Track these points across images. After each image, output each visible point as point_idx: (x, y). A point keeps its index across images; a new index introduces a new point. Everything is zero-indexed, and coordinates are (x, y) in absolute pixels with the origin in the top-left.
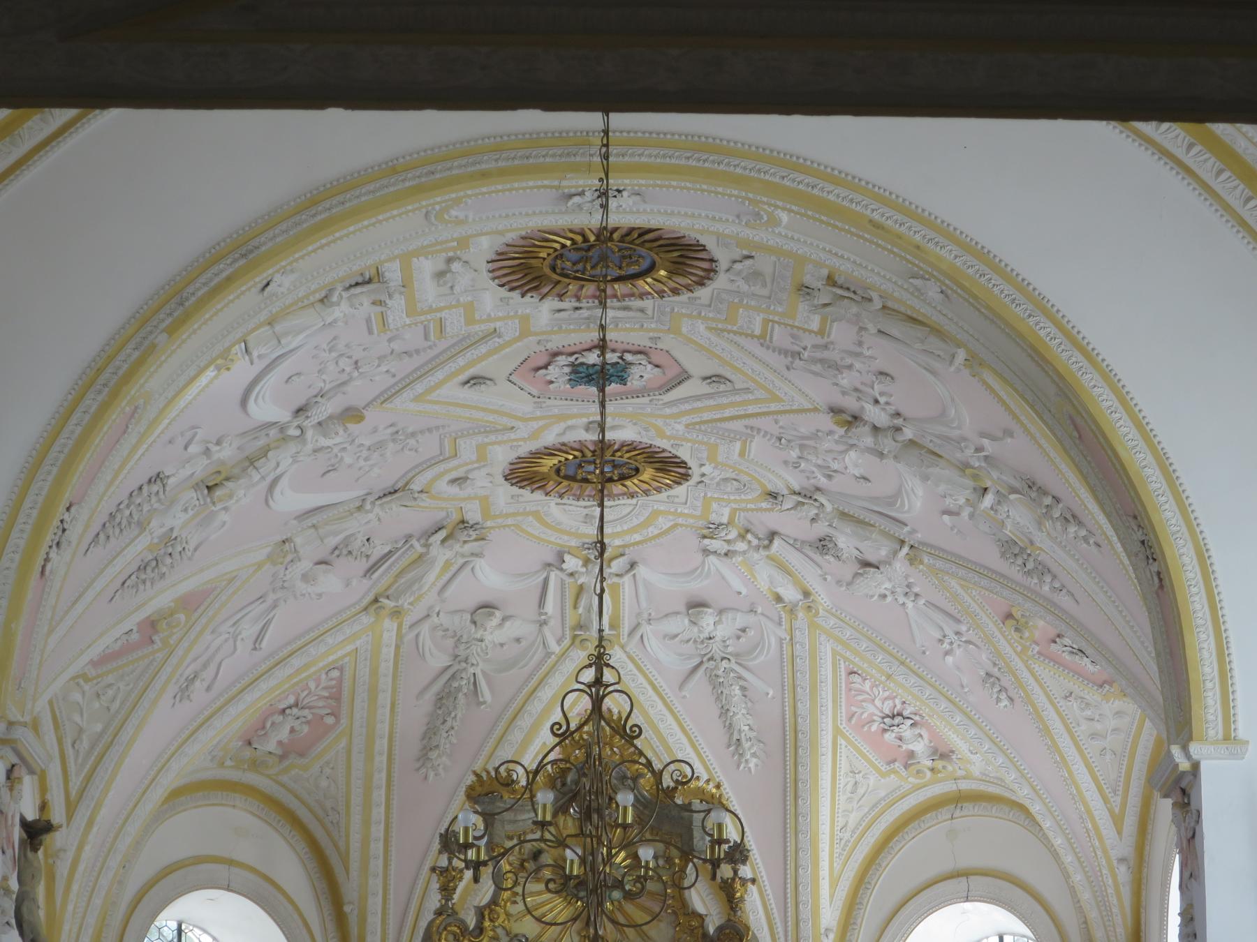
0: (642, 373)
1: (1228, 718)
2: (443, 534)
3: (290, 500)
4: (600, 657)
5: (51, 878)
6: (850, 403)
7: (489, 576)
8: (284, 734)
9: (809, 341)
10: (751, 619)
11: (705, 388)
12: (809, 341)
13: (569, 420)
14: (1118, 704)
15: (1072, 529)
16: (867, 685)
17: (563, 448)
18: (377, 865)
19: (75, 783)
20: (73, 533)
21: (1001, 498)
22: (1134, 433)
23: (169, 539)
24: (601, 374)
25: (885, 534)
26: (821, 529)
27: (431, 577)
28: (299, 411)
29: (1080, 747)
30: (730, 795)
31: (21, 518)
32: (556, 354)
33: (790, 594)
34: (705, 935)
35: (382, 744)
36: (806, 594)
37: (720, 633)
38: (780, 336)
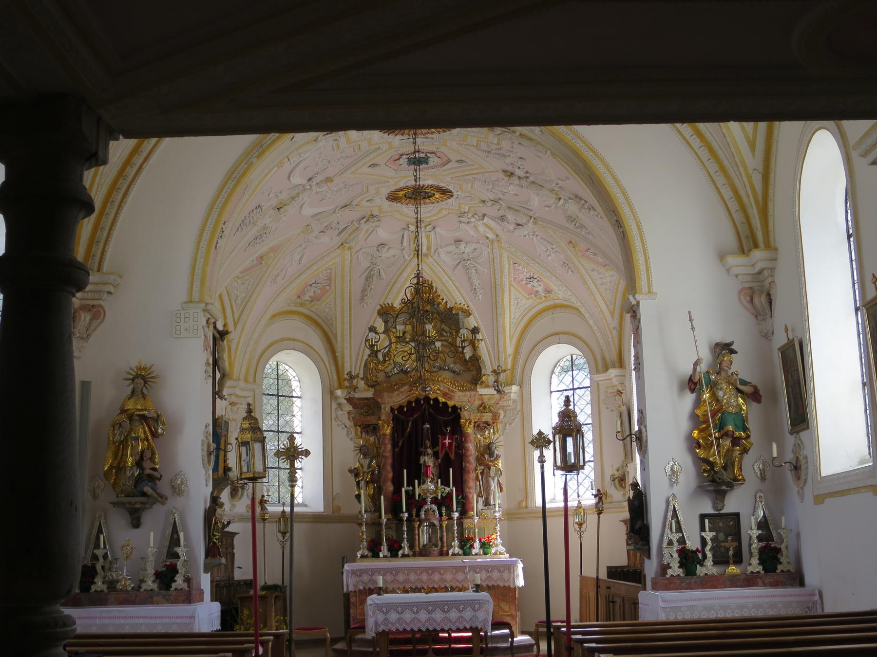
0: (433, 161)
1: (649, 285)
2: (365, 220)
3: (308, 211)
4: (418, 274)
5: (229, 349)
6: (510, 169)
7: (382, 234)
8: (311, 294)
9: (494, 147)
10: (478, 245)
11: (457, 165)
12: (494, 147)
13: (405, 178)
14: (611, 273)
15: (592, 212)
16: (520, 268)
17: (407, 188)
18: (347, 338)
19: (236, 315)
20: (227, 232)
21: (566, 201)
22: (612, 181)
23: (265, 228)
24: (417, 161)
25: (526, 215)
26: (501, 213)
27: (361, 235)
28: (310, 179)
29: (598, 289)
30: (473, 309)
31: (207, 228)
32: (402, 155)
33: (491, 236)
34: (465, 360)
35: (347, 295)
36: (497, 236)
37: (467, 251)
38: (483, 146)
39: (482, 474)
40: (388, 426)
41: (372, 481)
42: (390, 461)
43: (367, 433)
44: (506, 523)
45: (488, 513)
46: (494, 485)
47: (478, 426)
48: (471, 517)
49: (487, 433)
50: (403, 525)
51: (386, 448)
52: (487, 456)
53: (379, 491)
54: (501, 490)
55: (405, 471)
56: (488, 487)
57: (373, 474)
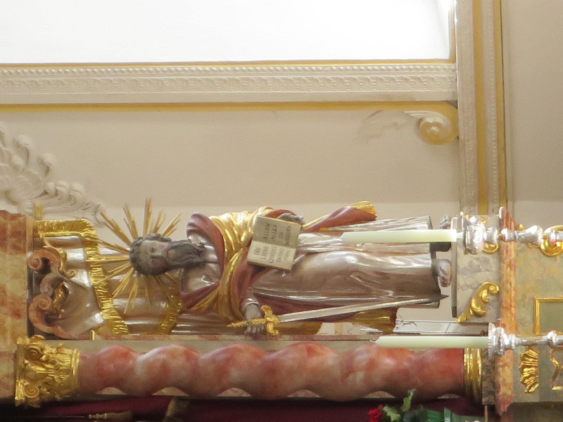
39: (282, 307)
44: (521, 207)
45: (472, 281)
46: (335, 253)
47: (50, 318)
48: (492, 360)
49: (84, 278)
52: (199, 282)
54: (364, 217)
56: (348, 282)
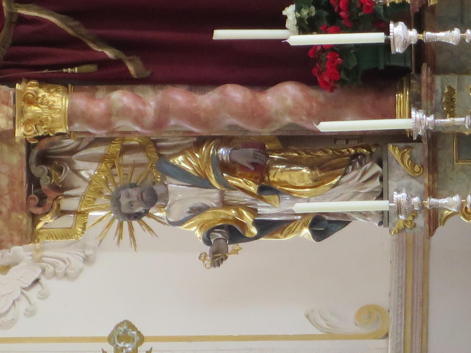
40: (32, 101)
41: (259, 171)
42: (179, 96)
43: (61, 189)
50: (442, 46)
51: (124, 113)
53: (298, 143)
55: (220, 34)
57: (227, 167)
